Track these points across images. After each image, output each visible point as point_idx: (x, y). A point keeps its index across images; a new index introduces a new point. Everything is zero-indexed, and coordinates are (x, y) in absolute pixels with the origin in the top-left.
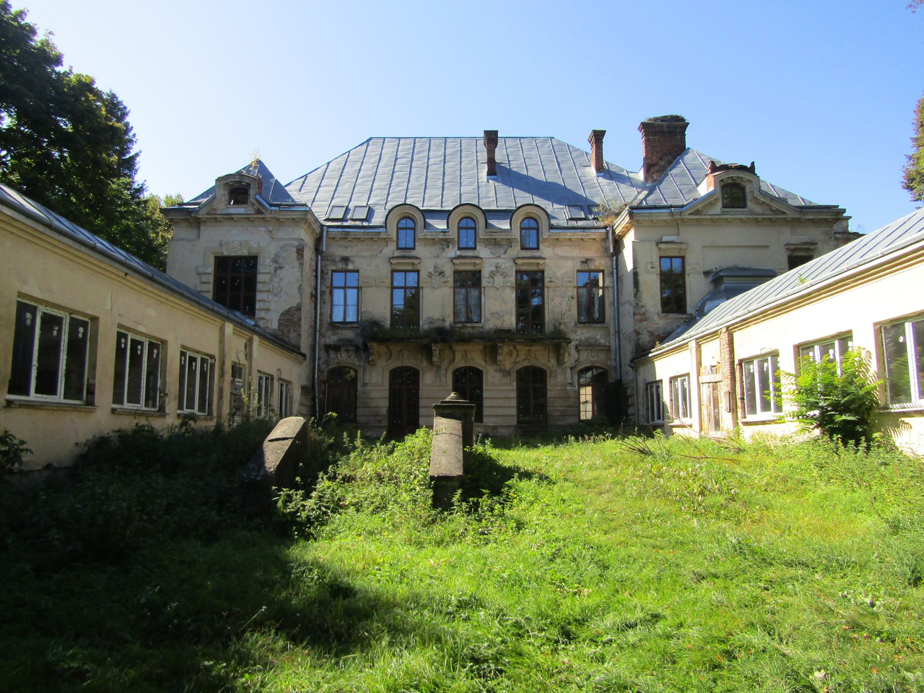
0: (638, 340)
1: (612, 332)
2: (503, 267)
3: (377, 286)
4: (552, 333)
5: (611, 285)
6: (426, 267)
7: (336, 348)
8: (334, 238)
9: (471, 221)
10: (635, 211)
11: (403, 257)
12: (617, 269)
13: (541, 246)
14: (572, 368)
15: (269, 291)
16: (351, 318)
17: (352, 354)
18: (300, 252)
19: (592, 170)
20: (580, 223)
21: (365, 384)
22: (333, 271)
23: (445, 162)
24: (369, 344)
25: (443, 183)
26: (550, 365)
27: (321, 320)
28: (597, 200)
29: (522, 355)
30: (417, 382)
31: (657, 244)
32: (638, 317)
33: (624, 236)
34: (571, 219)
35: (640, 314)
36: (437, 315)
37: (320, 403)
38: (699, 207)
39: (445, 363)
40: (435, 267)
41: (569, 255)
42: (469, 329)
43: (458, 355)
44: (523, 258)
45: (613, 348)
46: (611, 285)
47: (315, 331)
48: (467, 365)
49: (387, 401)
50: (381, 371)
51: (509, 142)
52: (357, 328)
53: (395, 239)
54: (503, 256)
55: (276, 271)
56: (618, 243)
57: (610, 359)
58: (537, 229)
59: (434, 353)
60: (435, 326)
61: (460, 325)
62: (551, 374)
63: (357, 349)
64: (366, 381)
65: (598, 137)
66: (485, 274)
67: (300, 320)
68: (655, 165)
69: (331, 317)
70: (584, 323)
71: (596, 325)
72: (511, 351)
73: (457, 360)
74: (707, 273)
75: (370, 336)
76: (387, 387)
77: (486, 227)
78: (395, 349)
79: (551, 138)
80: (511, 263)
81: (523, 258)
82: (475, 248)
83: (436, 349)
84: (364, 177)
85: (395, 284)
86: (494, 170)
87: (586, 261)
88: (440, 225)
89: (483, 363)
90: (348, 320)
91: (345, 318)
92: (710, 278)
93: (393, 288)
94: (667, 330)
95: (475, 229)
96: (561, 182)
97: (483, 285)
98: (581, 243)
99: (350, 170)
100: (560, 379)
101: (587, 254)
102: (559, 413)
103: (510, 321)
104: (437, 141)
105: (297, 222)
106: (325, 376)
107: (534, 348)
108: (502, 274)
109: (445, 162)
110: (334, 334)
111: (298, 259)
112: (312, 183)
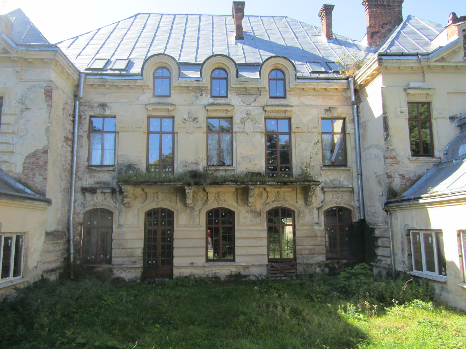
0: (390, 183)
1: (355, 175)
2: (253, 114)
3: (133, 131)
4: (299, 175)
5: (353, 131)
6: (181, 114)
7: (93, 191)
8: (92, 85)
9: (221, 72)
10: (383, 57)
11: (159, 104)
12: (358, 116)
13: (288, 95)
14: (318, 209)
15: (13, 133)
16: (108, 161)
17: (108, 196)
18: (49, 94)
19: (323, 38)
20: (322, 76)
21: (120, 226)
22: (91, 117)
23: (199, 31)
24: (123, 187)
25: (198, 45)
26: (298, 205)
27: (77, 164)
28: (332, 59)
29: (272, 197)
30: (171, 223)
31: (405, 90)
32: (389, 160)
33: (366, 85)
34: (314, 72)
35: (390, 157)
36: (191, 158)
37: (75, 245)
38: (444, 55)
39: (199, 205)
40: (189, 113)
41: (313, 103)
42: (221, 173)
43: (211, 197)
44: (272, 106)
45: (356, 190)
46: (353, 131)
47: (72, 174)
48: (220, 206)
49: (142, 242)
50: (136, 212)
51: (252, 19)
52: (114, 171)
53: (151, 86)
54: (253, 104)
55: (22, 112)
56: (359, 92)
57: (353, 200)
58: (284, 80)
59: (188, 195)
60: (189, 169)
61: (213, 168)
62: (299, 216)
63: (113, 191)
64: (122, 222)
65: (328, 10)
66: (237, 120)
67: (46, 163)
68: (378, 32)
69: (89, 159)
70: (329, 166)
71: (340, 168)
72: (261, 193)
73: (209, 202)
74: (452, 118)
75: (127, 179)
76: (143, 229)
77: (237, 77)
78: (150, 190)
79: (286, 17)
80: (261, 111)
81: (272, 106)
82: (226, 97)
83: (189, 191)
84: (128, 39)
85: (151, 129)
86: (240, 36)
87: (329, 109)
88: (196, 75)
89: (235, 204)
90: (105, 163)
91: (102, 161)
92: (456, 123)
93: (149, 133)
94: (417, 174)
95: (226, 79)
96: (298, 46)
97: (234, 130)
98: (325, 93)
99: (118, 34)
100: (308, 219)
101: (331, 103)
102: (307, 252)
103: (260, 165)
104: (193, 17)
105: (46, 63)
106: (81, 218)
107: (283, 190)
108: (252, 121)
109: (199, 31)
110: (90, 177)
111: (47, 100)
112: (81, 42)
